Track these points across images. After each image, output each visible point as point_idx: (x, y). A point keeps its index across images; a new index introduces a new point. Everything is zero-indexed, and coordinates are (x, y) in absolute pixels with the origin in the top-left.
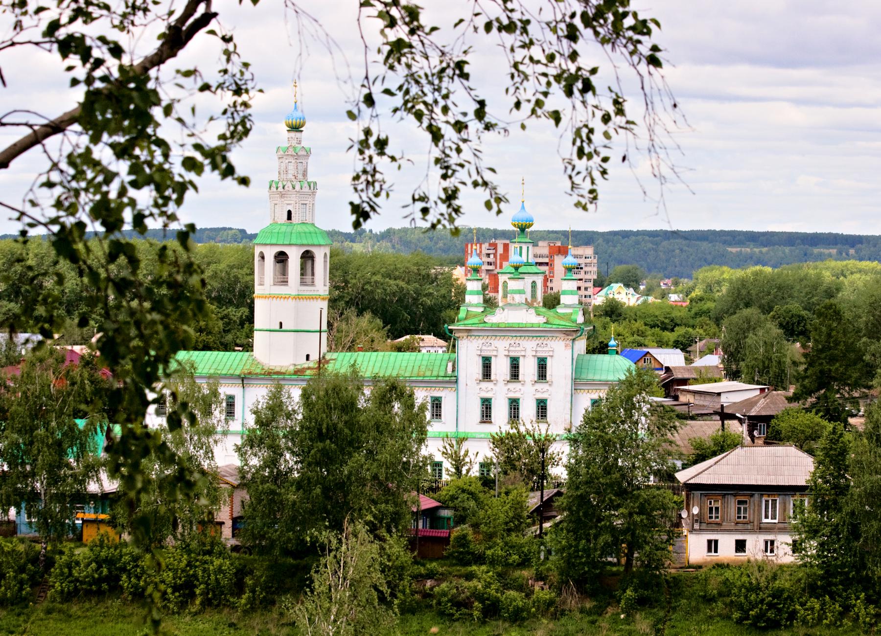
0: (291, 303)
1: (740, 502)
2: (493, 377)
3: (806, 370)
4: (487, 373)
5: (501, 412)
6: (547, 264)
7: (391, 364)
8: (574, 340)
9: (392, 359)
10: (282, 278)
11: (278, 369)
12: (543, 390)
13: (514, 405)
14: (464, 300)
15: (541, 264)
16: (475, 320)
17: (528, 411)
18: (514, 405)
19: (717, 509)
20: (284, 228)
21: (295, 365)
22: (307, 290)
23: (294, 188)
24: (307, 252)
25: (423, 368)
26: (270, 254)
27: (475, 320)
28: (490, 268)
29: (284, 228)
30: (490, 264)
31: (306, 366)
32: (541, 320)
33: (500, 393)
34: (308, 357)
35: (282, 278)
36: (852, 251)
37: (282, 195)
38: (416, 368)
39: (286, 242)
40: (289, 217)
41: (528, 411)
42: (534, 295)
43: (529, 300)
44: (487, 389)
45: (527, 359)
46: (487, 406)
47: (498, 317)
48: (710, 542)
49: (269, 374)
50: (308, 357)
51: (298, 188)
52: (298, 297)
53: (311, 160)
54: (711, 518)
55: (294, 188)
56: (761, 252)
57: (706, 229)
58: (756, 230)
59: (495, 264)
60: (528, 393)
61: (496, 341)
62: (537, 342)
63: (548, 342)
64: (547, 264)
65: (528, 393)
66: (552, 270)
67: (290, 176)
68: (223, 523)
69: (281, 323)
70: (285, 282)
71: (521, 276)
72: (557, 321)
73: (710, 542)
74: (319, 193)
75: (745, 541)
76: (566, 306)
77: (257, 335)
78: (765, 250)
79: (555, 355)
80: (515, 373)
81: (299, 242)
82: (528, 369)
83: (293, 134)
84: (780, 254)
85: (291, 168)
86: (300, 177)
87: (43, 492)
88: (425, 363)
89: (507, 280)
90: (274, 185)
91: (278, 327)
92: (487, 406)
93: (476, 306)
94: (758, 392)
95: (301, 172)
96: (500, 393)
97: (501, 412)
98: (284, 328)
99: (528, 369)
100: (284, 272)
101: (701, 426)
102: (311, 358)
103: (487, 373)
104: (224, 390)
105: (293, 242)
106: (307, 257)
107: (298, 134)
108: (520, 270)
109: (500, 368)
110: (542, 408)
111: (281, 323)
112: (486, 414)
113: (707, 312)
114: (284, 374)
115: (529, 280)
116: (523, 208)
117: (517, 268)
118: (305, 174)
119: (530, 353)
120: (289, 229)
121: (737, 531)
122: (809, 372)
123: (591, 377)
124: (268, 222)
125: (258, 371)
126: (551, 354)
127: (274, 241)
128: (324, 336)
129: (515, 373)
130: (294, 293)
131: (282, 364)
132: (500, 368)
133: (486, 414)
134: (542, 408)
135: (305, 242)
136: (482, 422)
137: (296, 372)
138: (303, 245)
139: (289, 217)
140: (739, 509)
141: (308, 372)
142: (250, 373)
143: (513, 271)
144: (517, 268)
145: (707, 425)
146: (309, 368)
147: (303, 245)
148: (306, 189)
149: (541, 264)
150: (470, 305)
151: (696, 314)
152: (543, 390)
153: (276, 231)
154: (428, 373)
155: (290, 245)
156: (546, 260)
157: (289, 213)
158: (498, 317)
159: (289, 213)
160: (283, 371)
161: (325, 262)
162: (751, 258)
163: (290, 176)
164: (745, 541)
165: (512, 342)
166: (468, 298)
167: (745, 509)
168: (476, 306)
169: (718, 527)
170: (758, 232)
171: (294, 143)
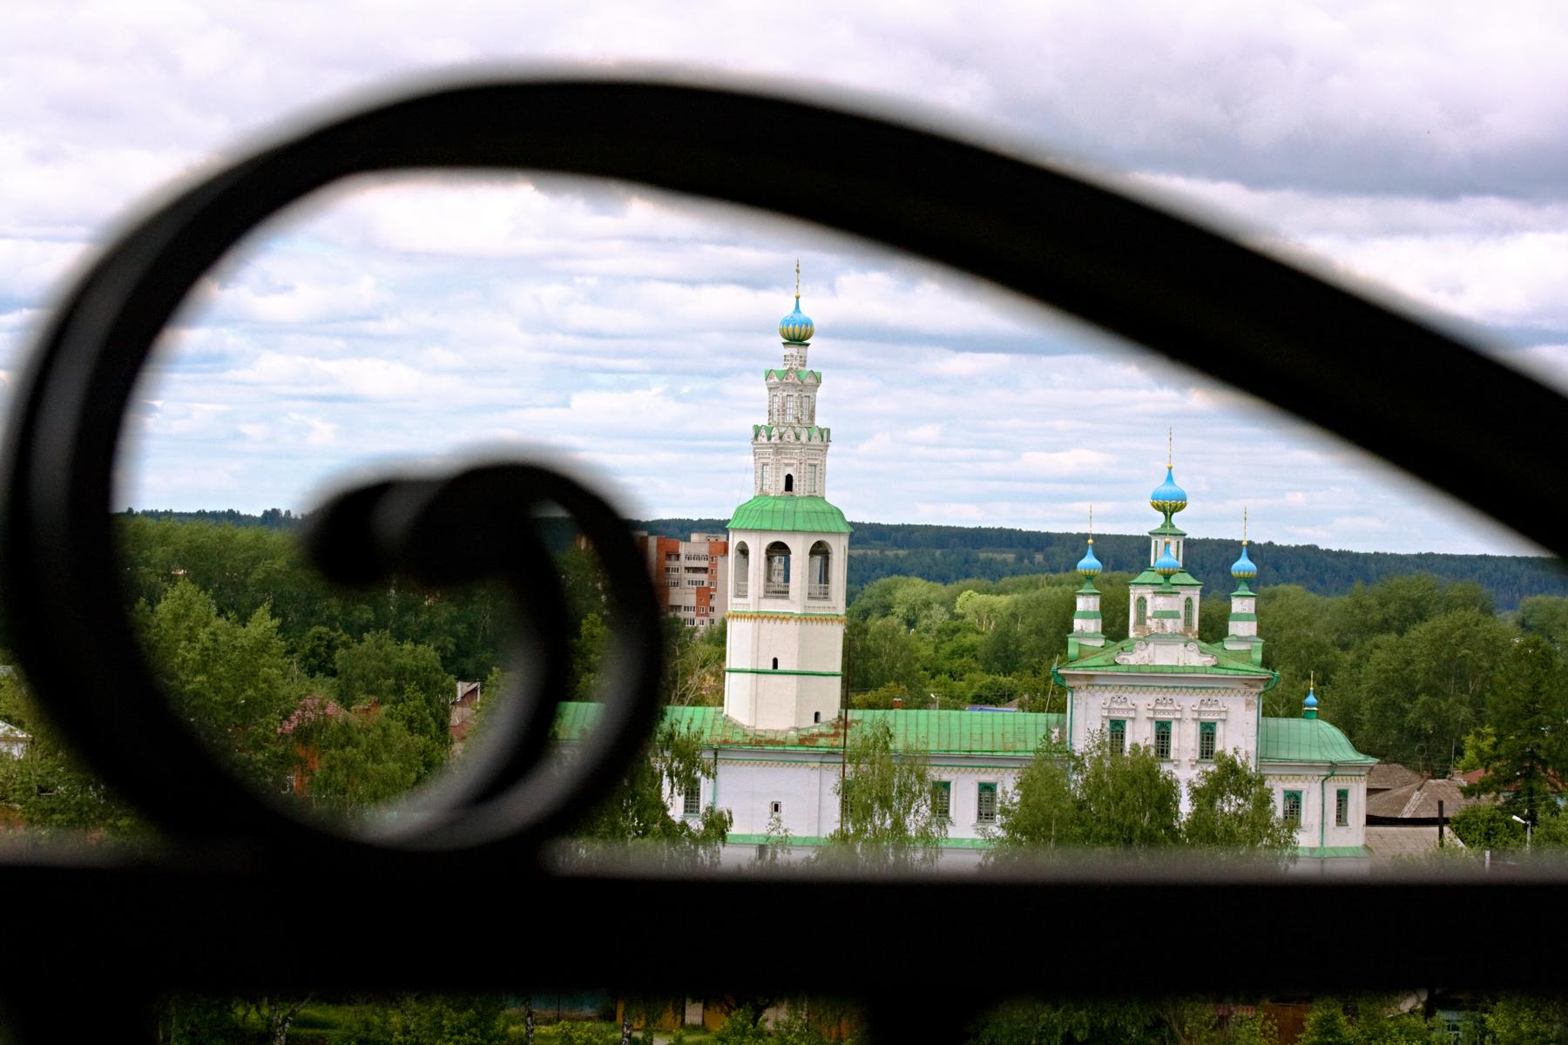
0: (793, 626)
2: (1172, 756)
3: (1495, 746)
6: (705, 570)
7: (955, 731)
9: (954, 721)
10: (777, 588)
11: (771, 736)
14: (1071, 630)
15: (696, 570)
16: (1099, 661)
20: (781, 505)
21: (798, 729)
22: (819, 607)
23: (798, 438)
24: (819, 544)
25: (1010, 738)
26: (758, 548)
27: (1099, 661)
29: (781, 505)
31: (816, 731)
32: (1207, 660)
35: (777, 588)
36: (1039, 557)
37: (778, 450)
38: (998, 737)
39: (787, 527)
42: (1188, 623)
45: (1183, 726)
47: (1137, 656)
49: (758, 743)
51: (804, 438)
52: (804, 618)
53: (821, 392)
55: (798, 438)
56: (897, 556)
58: (884, 522)
61: (1134, 695)
62: (1201, 697)
63: (1219, 698)
64: (705, 570)
67: (790, 419)
69: (775, 661)
71: (1175, 589)
72: (1233, 664)
74: (832, 448)
76: (1240, 639)
77: (731, 680)
78: (902, 553)
79: (1231, 717)
81: (808, 527)
83: (793, 350)
84: (928, 560)
85: (791, 404)
86: (805, 419)
88: (1010, 729)
89: (1148, 597)
90: (764, 433)
91: (770, 667)
93: (1093, 636)
95: (806, 412)
98: (780, 667)
100: (825, 577)
101: (1394, 835)
102: (822, 718)
104: (935, 774)
105: (799, 526)
106: (778, 550)
107: (802, 350)
108: (1173, 580)
111: (775, 661)
113: (971, 650)
114: (783, 743)
115: (1185, 593)
116: (1170, 478)
117: (1167, 576)
118: (812, 417)
120: (789, 506)
122: (1502, 750)
123: (1283, 755)
124: (748, 494)
125: (739, 738)
126: (1223, 716)
127: (767, 525)
130: (798, 611)
131: (776, 727)
135: (817, 528)
137: (802, 742)
138: (814, 532)
141: (822, 741)
142: (726, 742)
143: (1161, 580)
144: (1167, 576)
146: (821, 735)
147: (814, 532)
148: (816, 441)
149: (696, 570)
150: (1083, 635)
151: (953, 652)
153: (769, 507)
154: (1020, 746)
155: (794, 531)
156: (704, 564)
157: (789, 479)
158: (1137, 656)
159: (789, 479)
160: (780, 738)
162: (882, 565)
163: (790, 419)
165: (1160, 696)
166: (1078, 624)
168: (1093, 636)
170: (888, 526)
171: (795, 364)
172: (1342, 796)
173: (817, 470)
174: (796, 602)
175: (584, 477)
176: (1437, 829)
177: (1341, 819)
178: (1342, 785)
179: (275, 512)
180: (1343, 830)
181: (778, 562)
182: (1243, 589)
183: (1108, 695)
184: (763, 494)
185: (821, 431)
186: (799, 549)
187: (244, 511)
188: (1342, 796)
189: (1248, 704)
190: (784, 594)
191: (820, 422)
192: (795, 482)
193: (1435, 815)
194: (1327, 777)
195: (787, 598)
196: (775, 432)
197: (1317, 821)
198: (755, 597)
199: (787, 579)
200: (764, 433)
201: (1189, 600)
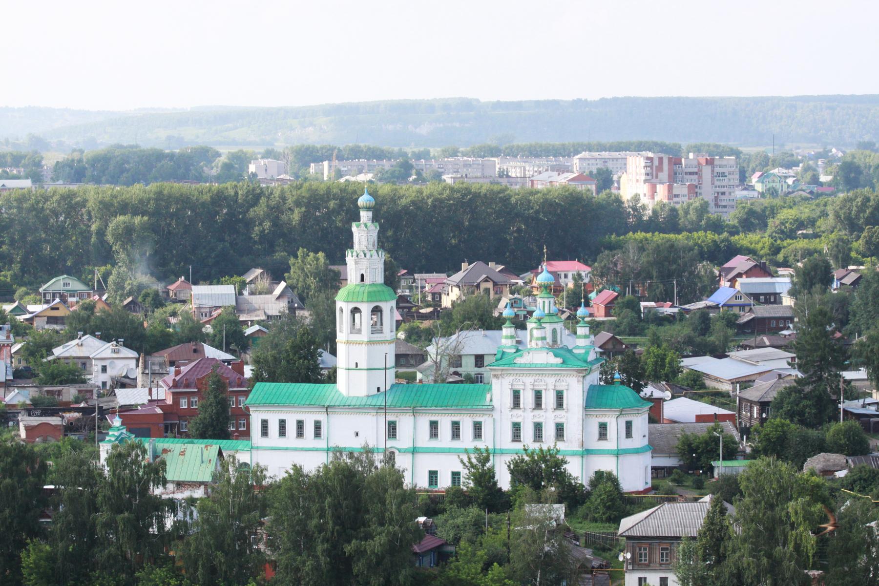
1: (663, 549)
4: (516, 404)
5: (527, 433)
8: (584, 377)
12: (561, 416)
13: (538, 428)
15: (691, 173)
17: (549, 432)
18: (538, 428)
19: (645, 554)
33: (527, 418)
34: (378, 389)
35: (354, 329)
40: (362, 279)
41: (549, 432)
44: (518, 416)
45: (548, 392)
46: (517, 427)
48: (640, 579)
50: (378, 389)
57: (848, 93)
60: (549, 417)
64: (696, 173)
65: (549, 417)
66: (700, 177)
73: (640, 579)
75: (667, 578)
80: (538, 404)
82: (549, 399)
91: (354, 367)
92: (517, 427)
96: (527, 418)
97: (527, 433)
99: (549, 399)
103: (516, 404)
109: (527, 399)
110: (560, 430)
112: (516, 436)
119: (551, 387)
121: (661, 570)
129: (538, 404)
132: (527, 399)
133: (516, 436)
134: (560, 430)
136: (513, 441)
139: (362, 279)
140: (662, 554)
145: (773, 308)
149: (691, 173)
152: (561, 416)
156: (696, 170)
157: (362, 276)
159: (362, 276)
164: (667, 578)
167: (667, 554)
168: (510, 348)
169: (647, 567)
172: (629, 425)
174: (365, 336)
175: (104, 141)
177: (629, 434)
178: (629, 419)
180: (630, 440)
181: (357, 315)
182: (508, 324)
183: (511, 378)
186: (366, 309)
188: (629, 425)
189: (578, 381)
190: (359, 331)
199: (382, 324)
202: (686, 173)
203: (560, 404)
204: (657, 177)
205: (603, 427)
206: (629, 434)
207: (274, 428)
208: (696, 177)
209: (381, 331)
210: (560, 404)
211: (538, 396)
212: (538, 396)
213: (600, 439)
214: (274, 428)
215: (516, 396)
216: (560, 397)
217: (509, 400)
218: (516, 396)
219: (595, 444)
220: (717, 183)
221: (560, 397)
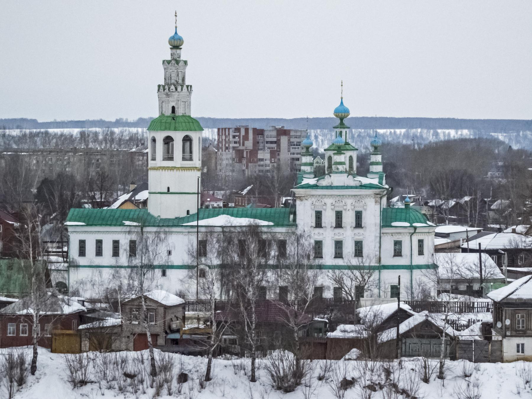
6: (275, 142)
13: (339, 244)
17: (349, 249)
18: (339, 244)
22: (188, 164)
28: (237, 145)
30: (235, 143)
43: (348, 169)
48: (518, 346)
54: (519, 327)
59: (239, 143)
60: (348, 236)
66: (279, 146)
67: (173, 81)
68: (159, 335)
69: (168, 188)
70: (171, 159)
80: (339, 224)
82: (349, 219)
87: (35, 316)
89: (332, 156)
91: (166, 191)
94: (476, 233)
95: (181, 78)
98: (171, 191)
99: (349, 219)
102: (191, 213)
111: (168, 188)
118: (183, 80)
128: (200, 195)
129: (339, 224)
132: (329, 218)
152: (359, 234)
159: (173, 108)
161: (199, 143)
173: (187, 104)
176: (478, 254)
179: (121, 119)
180: (421, 256)
181: (188, 144)
184: (162, 115)
185: (187, 86)
187: (107, 120)
189: (376, 202)
191: (187, 83)
192: (176, 109)
193: (478, 248)
194: (413, 234)
195: (173, 160)
196: (167, 87)
197: (409, 254)
198: (160, 162)
200: (161, 88)
201: (351, 158)
202: (267, 142)
203: (359, 224)
204: (243, 145)
205: (398, 244)
206: (421, 253)
207: (91, 248)
208: (274, 146)
209: (191, 159)
210: (359, 224)
211: (339, 216)
212: (339, 216)
213: (395, 256)
214: (91, 248)
215: (319, 215)
216: (359, 216)
217: (312, 221)
218: (319, 215)
219: (388, 259)
220: (292, 151)
221: (359, 216)
